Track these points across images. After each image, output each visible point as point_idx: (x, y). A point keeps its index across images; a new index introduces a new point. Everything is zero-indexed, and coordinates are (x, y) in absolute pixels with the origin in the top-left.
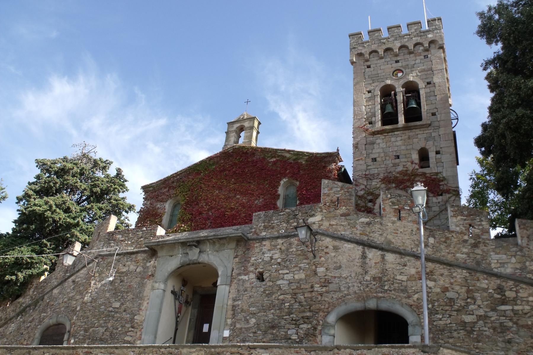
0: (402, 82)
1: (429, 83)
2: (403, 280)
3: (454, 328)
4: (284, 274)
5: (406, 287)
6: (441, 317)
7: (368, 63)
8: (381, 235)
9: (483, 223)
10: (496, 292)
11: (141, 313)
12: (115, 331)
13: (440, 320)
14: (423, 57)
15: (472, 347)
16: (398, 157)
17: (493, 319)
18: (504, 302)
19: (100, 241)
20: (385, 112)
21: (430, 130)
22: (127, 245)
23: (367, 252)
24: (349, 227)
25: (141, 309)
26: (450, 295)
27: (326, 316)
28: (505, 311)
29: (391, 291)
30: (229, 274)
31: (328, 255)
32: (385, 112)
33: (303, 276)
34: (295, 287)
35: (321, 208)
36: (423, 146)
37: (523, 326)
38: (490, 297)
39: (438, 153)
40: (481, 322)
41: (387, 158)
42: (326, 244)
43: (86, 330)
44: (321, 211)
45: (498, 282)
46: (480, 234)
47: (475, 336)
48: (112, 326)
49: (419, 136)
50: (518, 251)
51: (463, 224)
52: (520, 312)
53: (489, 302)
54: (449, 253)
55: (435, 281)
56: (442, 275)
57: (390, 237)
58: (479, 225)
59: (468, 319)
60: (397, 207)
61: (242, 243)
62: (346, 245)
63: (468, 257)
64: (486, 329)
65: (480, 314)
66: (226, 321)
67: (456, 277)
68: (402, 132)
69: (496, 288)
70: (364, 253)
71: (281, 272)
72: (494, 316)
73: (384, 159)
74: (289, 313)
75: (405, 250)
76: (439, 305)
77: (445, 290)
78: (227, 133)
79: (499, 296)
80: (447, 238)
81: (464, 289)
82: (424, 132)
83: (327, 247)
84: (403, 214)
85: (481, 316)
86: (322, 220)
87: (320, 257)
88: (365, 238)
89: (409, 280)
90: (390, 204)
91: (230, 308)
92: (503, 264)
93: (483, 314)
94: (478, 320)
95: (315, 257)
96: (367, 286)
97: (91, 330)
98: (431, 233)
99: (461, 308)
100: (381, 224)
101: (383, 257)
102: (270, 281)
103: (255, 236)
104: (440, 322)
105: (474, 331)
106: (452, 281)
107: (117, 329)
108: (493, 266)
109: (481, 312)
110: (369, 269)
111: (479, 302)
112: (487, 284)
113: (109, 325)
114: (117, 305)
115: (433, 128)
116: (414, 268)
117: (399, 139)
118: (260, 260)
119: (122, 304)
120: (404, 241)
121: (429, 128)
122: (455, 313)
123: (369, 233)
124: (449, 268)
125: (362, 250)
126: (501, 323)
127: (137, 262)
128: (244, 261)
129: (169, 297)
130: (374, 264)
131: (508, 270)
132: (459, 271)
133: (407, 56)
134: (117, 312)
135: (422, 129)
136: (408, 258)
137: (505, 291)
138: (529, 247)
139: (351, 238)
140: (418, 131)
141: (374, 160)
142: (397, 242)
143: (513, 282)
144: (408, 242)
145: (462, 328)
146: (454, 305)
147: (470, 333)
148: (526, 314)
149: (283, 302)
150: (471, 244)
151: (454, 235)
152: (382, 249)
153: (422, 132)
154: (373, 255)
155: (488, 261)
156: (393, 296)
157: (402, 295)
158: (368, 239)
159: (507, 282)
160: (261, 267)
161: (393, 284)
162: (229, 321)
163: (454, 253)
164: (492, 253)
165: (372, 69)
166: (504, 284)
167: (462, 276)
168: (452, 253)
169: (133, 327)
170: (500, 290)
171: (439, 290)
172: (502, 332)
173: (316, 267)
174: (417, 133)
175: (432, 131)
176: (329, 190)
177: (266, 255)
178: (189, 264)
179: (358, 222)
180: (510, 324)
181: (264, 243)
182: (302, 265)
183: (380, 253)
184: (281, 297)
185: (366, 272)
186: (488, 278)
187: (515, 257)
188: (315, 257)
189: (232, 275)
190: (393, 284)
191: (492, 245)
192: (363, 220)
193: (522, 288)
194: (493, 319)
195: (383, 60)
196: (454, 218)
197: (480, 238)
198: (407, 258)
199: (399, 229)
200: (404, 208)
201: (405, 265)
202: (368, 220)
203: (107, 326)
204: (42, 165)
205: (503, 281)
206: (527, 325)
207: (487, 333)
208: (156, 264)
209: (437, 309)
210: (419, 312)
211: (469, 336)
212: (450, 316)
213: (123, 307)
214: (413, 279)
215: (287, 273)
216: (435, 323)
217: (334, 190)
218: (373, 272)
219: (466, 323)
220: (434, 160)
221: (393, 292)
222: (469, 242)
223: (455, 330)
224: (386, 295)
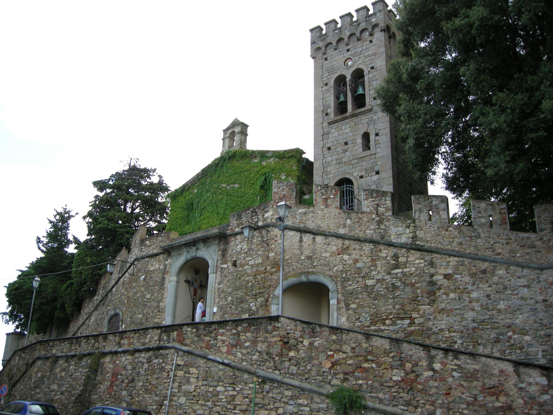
0: (351, 71)
1: (372, 68)
2: (327, 256)
3: (359, 291)
4: (249, 261)
5: (328, 262)
6: (351, 283)
7: (325, 56)
8: (313, 221)
9: (388, 202)
10: (392, 259)
11: (164, 300)
12: (148, 316)
13: (351, 285)
14: (368, 42)
15: (371, 304)
16: (346, 144)
17: (387, 281)
18: (397, 267)
19: (136, 247)
20: (357, 94)
21: (370, 115)
22: (153, 249)
23: (303, 237)
24: (291, 218)
25: (163, 298)
26: (359, 265)
27: (274, 290)
28: (397, 274)
29: (318, 266)
30: (215, 265)
31: (277, 242)
32: (357, 94)
33: (260, 261)
34: (255, 270)
35: (272, 205)
36: (365, 131)
37: (408, 285)
38: (388, 264)
39: (377, 135)
40: (379, 284)
41: (339, 145)
42: (276, 233)
43: (131, 318)
44: (272, 207)
45: (395, 250)
46: (384, 212)
47: (373, 296)
48: (146, 313)
49: (363, 122)
50: (411, 223)
51: (372, 205)
52: (408, 273)
53: (387, 268)
54: (360, 231)
55: (350, 255)
56: (355, 249)
57: (319, 222)
58: (384, 204)
59: (370, 282)
60: (325, 197)
61: (223, 239)
62: (289, 233)
63: (375, 232)
64: (382, 289)
65: (379, 278)
66: (214, 300)
67: (364, 250)
68: (350, 119)
69: (393, 255)
70: (301, 238)
71: (247, 259)
72: (388, 278)
73: (336, 147)
74: (252, 291)
75: (329, 232)
76: (351, 274)
77: (356, 261)
78: (223, 139)
79: (394, 262)
80: (360, 218)
81: (370, 259)
82: (367, 117)
83: (276, 236)
84: (329, 202)
85: (379, 280)
86: (273, 214)
87: (272, 245)
88: (302, 225)
89: (331, 256)
90: (320, 195)
91: (216, 290)
92: (399, 235)
93: (380, 278)
94: (377, 283)
95: (268, 245)
96: (302, 264)
97: (134, 317)
98: (349, 216)
99: (365, 275)
100: (313, 212)
101: (314, 238)
102: (240, 267)
103: (232, 232)
104: (350, 287)
105: (374, 292)
106: (362, 253)
107: (150, 314)
108: (392, 237)
109: (380, 277)
110: (304, 251)
111: (379, 269)
112: (386, 253)
113: (145, 312)
114: (148, 296)
115: (374, 112)
116: (335, 246)
117: (348, 126)
118: (235, 251)
119: (152, 295)
120: (329, 225)
121: (371, 113)
122: (361, 279)
123: (305, 221)
124: (360, 243)
125: (300, 235)
126: (393, 283)
127: (160, 261)
128: (224, 253)
129: (184, 286)
130: (307, 246)
131: (403, 240)
132: (367, 244)
133: (356, 44)
134: (148, 302)
135: (365, 115)
136: (331, 238)
137: (399, 258)
138: (420, 218)
139: (292, 226)
140: (363, 117)
141: (329, 149)
142: (323, 226)
143: (405, 250)
144: (332, 225)
145: (365, 290)
146: (361, 273)
147: (370, 293)
148: (412, 274)
149: (248, 282)
150: (377, 221)
151: (365, 215)
152: (314, 234)
153: (365, 117)
154: (307, 238)
155: (389, 234)
156: (318, 270)
157: (325, 268)
158: (304, 226)
159: (401, 250)
160: (235, 256)
161: (319, 261)
162: (217, 300)
163: (364, 231)
164: (392, 227)
165: (328, 62)
166: (398, 252)
167: (369, 249)
168: (363, 231)
169: (159, 312)
170: (396, 257)
171: (351, 262)
172: (393, 291)
173: (269, 253)
174: (361, 119)
175: (373, 115)
176: (278, 189)
177: (238, 247)
178: (191, 260)
179: (297, 213)
180: (399, 284)
181: (237, 237)
182: (260, 252)
183: (312, 236)
184: (247, 279)
185: (302, 253)
186: (388, 248)
187: (409, 228)
188: (268, 245)
189: (217, 266)
190: (319, 261)
191: (393, 220)
192: (301, 210)
193: (411, 253)
194: (387, 281)
195: (337, 50)
196: (366, 201)
197: (384, 215)
198: (330, 239)
199: (326, 215)
200: (330, 197)
201: (329, 245)
202: (304, 210)
203: (144, 313)
204: (100, 185)
205: (398, 250)
206: (412, 283)
207: (382, 293)
208: (171, 262)
209: (349, 277)
210: (337, 281)
211: (369, 296)
212: (358, 281)
213: (153, 297)
214: (334, 255)
215: (251, 260)
216: (346, 289)
217: (281, 188)
218: (307, 252)
219: (367, 286)
220: (374, 142)
221: (319, 267)
222: (376, 220)
223: (360, 293)
224: (314, 270)
